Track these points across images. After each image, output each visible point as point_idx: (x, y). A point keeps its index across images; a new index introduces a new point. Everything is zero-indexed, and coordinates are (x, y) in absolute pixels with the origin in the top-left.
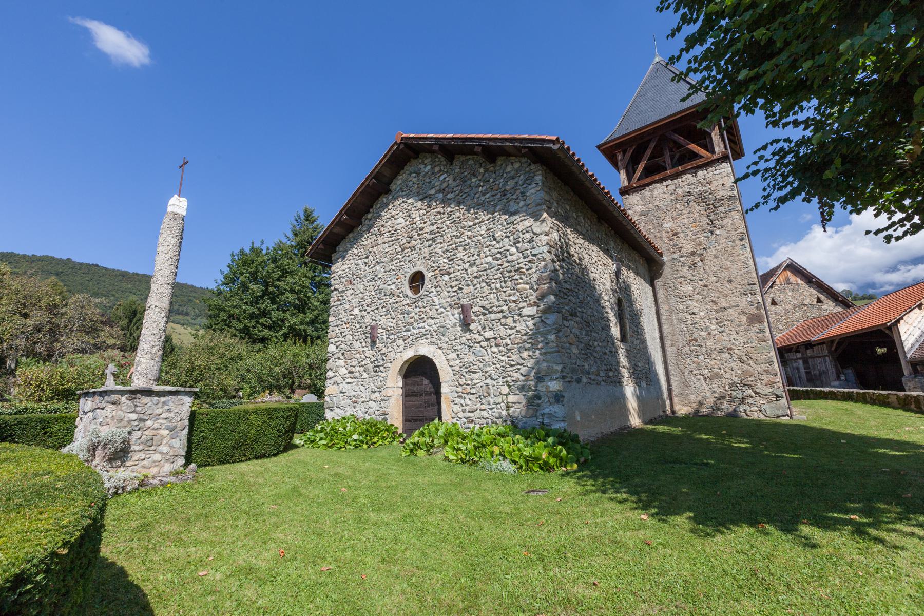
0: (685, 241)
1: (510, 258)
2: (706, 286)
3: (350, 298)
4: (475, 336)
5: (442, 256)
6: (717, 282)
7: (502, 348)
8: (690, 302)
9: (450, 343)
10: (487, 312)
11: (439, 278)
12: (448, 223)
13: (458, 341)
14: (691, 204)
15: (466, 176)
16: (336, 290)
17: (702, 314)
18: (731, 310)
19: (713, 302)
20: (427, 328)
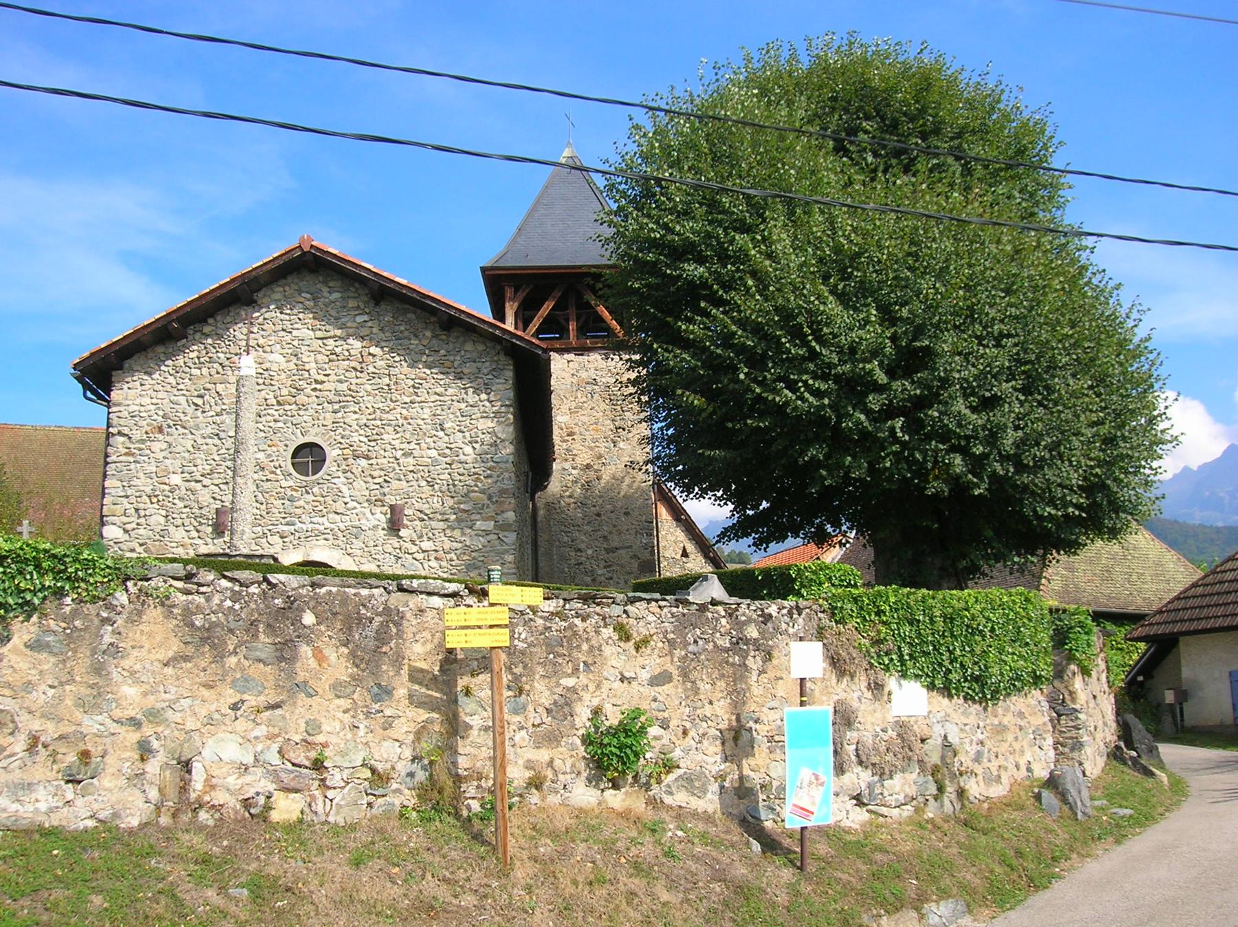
0: (582, 448)
1: (462, 458)
2: (599, 515)
3: (160, 456)
4: (406, 544)
5: (357, 431)
6: (612, 512)
7: (444, 564)
8: (577, 534)
9: (366, 549)
10: (426, 518)
11: (351, 461)
12: (369, 388)
13: (380, 548)
14: (596, 396)
15: (402, 332)
16: (120, 433)
17: (590, 552)
18: (622, 552)
19: (605, 537)
20: (327, 525)
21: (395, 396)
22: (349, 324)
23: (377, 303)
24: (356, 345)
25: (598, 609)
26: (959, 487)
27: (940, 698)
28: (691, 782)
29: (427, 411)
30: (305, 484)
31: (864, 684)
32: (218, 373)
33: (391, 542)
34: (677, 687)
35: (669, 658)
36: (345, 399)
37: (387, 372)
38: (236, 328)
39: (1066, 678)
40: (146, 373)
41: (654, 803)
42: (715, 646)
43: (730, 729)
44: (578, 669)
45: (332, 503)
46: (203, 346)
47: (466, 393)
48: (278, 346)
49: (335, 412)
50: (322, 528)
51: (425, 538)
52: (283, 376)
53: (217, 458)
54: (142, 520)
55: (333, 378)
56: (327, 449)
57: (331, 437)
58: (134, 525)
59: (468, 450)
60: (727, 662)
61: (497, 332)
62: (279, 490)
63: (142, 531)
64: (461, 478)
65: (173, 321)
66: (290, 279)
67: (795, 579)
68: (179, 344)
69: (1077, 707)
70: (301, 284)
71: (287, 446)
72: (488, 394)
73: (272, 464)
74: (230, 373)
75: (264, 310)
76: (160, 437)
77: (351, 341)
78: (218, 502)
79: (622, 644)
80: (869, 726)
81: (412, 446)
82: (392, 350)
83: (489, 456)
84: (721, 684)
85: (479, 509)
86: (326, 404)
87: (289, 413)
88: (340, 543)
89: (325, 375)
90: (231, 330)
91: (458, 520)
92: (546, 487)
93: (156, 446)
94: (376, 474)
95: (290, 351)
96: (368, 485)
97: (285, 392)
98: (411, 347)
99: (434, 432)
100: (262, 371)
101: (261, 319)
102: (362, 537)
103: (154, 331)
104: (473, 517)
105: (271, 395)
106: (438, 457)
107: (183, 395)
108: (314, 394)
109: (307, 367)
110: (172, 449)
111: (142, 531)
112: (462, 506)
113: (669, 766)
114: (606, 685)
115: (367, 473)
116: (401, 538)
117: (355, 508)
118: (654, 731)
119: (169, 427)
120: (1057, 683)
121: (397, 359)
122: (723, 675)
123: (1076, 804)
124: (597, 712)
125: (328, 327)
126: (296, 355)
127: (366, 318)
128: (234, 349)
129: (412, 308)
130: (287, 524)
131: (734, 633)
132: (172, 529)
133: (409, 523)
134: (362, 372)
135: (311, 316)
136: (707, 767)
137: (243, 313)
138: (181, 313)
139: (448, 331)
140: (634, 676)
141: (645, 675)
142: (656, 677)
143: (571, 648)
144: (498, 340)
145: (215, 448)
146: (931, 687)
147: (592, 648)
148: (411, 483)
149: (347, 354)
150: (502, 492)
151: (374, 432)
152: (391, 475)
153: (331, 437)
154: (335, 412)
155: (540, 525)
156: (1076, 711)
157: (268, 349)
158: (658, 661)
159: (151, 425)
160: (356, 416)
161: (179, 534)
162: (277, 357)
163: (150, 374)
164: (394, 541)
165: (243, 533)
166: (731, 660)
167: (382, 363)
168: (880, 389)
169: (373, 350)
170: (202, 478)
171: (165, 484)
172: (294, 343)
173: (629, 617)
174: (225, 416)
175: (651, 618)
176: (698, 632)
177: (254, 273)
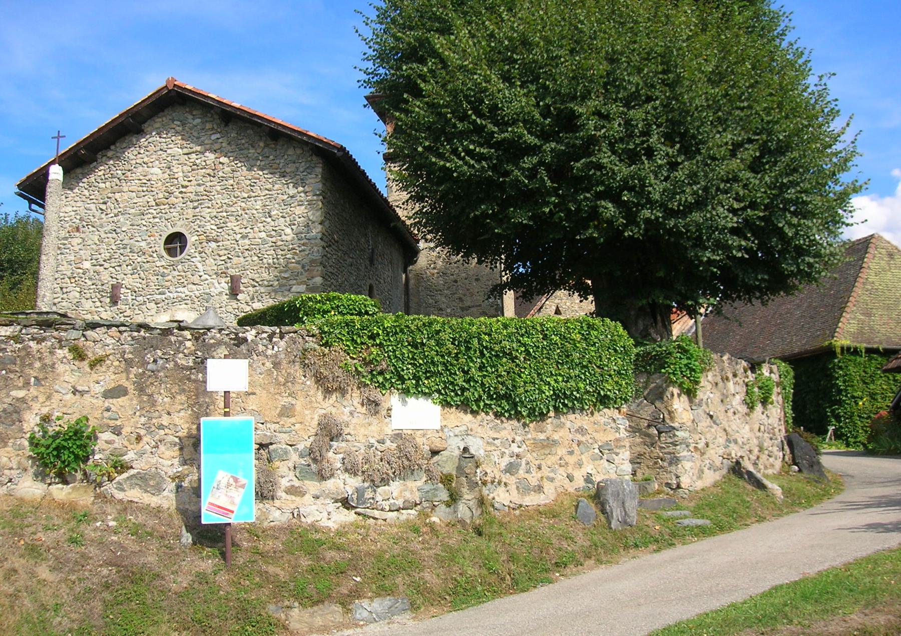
1: (284, 237)
2: (456, 281)
3: (77, 248)
5: (209, 221)
6: (466, 279)
10: (257, 284)
12: (218, 188)
15: (243, 144)
17: (449, 310)
19: (460, 299)
21: (237, 193)
22: (206, 142)
23: (226, 125)
24: (211, 156)
25: (55, 334)
26: (614, 233)
27: (462, 415)
28: (145, 481)
29: (259, 203)
30: (172, 263)
31: (356, 401)
32: (117, 185)
33: (231, 304)
34: (132, 400)
35: (124, 375)
36: (202, 198)
37: (231, 175)
38: (129, 151)
39: (666, 399)
40: (69, 189)
41: (104, 498)
42: (176, 364)
43: (189, 436)
44: (29, 383)
45: (191, 276)
46: (107, 167)
47: (288, 187)
48: (157, 162)
49: (194, 208)
50: (183, 295)
51: (256, 300)
52: (160, 183)
53: (114, 248)
54: (65, 296)
55: (194, 183)
56: (188, 236)
57: (191, 227)
58: (59, 300)
59: (288, 231)
60: (189, 379)
61: (305, 138)
62: (155, 268)
63: (64, 304)
64: (283, 252)
65: (81, 149)
66: (166, 112)
67: (300, 309)
68: (92, 166)
69: (676, 425)
70: (174, 114)
71: (161, 235)
72: (304, 187)
73: (150, 250)
74: (124, 184)
75: (148, 136)
76: (77, 234)
77: (207, 154)
78: (114, 280)
79: (77, 363)
80: (361, 438)
81: (248, 230)
82: (236, 159)
83: (303, 235)
84: (182, 398)
85: (295, 275)
86: (189, 203)
87: (163, 211)
88: (195, 306)
89: (189, 181)
90: (126, 153)
91: (281, 286)
92: (416, 261)
93: (75, 241)
94: (221, 253)
95: (165, 165)
96: (216, 262)
97: (161, 196)
98: (249, 155)
99: (264, 219)
100: (145, 181)
101: (146, 143)
102: (211, 301)
103: (69, 157)
104: (291, 282)
105: (152, 199)
106: (266, 238)
107: (94, 203)
108: (180, 195)
109: (176, 176)
110: (85, 243)
111: (64, 304)
112: (283, 275)
113: (121, 467)
114: (57, 397)
115: (215, 253)
116: (239, 300)
117: (207, 280)
118: (106, 436)
119: (84, 227)
120: (658, 404)
121: (239, 165)
122: (184, 390)
123: (612, 514)
124: (46, 419)
125: (192, 145)
126: (169, 168)
127: (218, 136)
128: (127, 167)
129: (251, 126)
130: (160, 294)
131: (200, 354)
132: (83, 301)
133: (244, 289)
134: (214, 177)
135: (180, 138)
136: (164, 469)
137: (134, 140)
138: (87, 142)
139: (276, 141)
140: (87, 389)
141: (98, 389)
142: (110, 391)
143: (23, 365)
144: (306, 143)
145: (114, 241)
146: (446, 404)
147: (44, 366)
148: (247, 259)
149: (204, 164)
150: (312, 262)
151: (221, 221)
152: (232, 253)
153: (191, 227)
154: (194, 208)
155: (411, 291)
156: (674, 428)
157: (150, 165)
158: (113, 377)
159: (72, 226)
160: (209, 210)
161: (88, 305)
162: (156, 170)
163: (71, 189)
164: (234, 304)
165: (44, 296)
166: (193, 377)
167: (229, 169)
168: (532, 150)
169: (223, 159)
170: (104, 263)
171: (80, 268)
172: (168, 159)
173: (87, 340)
174: (120, 216)
175: (109, 341)
176: (159, 353)
177: (135, 109)
